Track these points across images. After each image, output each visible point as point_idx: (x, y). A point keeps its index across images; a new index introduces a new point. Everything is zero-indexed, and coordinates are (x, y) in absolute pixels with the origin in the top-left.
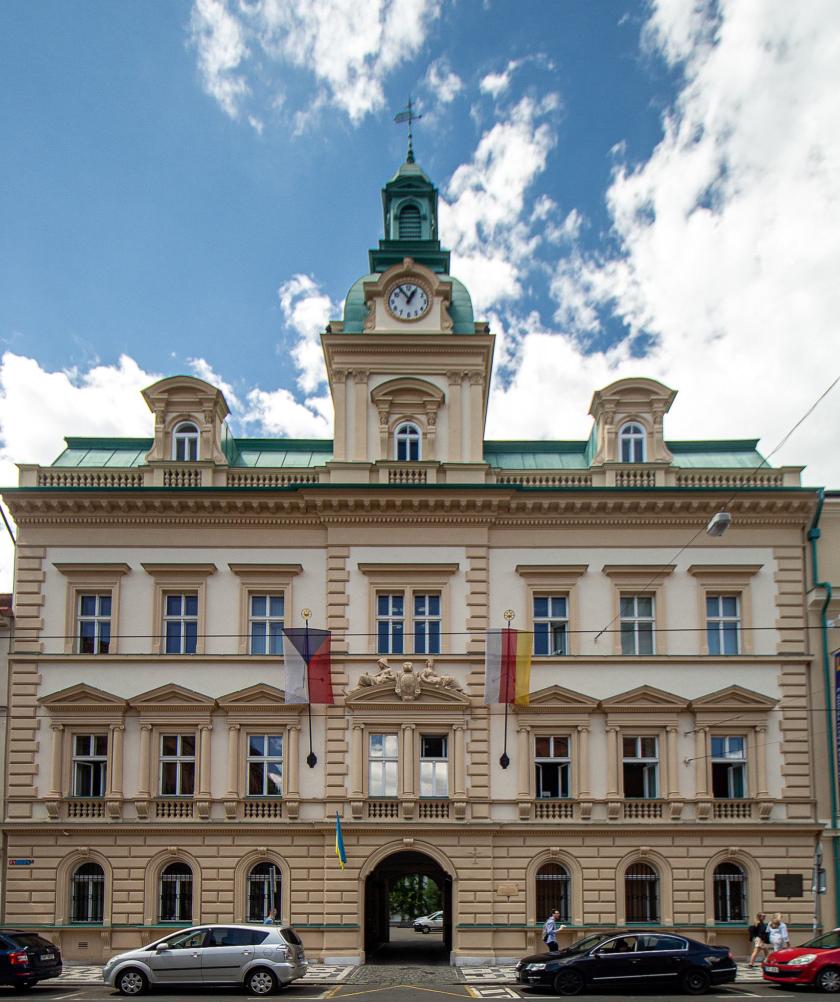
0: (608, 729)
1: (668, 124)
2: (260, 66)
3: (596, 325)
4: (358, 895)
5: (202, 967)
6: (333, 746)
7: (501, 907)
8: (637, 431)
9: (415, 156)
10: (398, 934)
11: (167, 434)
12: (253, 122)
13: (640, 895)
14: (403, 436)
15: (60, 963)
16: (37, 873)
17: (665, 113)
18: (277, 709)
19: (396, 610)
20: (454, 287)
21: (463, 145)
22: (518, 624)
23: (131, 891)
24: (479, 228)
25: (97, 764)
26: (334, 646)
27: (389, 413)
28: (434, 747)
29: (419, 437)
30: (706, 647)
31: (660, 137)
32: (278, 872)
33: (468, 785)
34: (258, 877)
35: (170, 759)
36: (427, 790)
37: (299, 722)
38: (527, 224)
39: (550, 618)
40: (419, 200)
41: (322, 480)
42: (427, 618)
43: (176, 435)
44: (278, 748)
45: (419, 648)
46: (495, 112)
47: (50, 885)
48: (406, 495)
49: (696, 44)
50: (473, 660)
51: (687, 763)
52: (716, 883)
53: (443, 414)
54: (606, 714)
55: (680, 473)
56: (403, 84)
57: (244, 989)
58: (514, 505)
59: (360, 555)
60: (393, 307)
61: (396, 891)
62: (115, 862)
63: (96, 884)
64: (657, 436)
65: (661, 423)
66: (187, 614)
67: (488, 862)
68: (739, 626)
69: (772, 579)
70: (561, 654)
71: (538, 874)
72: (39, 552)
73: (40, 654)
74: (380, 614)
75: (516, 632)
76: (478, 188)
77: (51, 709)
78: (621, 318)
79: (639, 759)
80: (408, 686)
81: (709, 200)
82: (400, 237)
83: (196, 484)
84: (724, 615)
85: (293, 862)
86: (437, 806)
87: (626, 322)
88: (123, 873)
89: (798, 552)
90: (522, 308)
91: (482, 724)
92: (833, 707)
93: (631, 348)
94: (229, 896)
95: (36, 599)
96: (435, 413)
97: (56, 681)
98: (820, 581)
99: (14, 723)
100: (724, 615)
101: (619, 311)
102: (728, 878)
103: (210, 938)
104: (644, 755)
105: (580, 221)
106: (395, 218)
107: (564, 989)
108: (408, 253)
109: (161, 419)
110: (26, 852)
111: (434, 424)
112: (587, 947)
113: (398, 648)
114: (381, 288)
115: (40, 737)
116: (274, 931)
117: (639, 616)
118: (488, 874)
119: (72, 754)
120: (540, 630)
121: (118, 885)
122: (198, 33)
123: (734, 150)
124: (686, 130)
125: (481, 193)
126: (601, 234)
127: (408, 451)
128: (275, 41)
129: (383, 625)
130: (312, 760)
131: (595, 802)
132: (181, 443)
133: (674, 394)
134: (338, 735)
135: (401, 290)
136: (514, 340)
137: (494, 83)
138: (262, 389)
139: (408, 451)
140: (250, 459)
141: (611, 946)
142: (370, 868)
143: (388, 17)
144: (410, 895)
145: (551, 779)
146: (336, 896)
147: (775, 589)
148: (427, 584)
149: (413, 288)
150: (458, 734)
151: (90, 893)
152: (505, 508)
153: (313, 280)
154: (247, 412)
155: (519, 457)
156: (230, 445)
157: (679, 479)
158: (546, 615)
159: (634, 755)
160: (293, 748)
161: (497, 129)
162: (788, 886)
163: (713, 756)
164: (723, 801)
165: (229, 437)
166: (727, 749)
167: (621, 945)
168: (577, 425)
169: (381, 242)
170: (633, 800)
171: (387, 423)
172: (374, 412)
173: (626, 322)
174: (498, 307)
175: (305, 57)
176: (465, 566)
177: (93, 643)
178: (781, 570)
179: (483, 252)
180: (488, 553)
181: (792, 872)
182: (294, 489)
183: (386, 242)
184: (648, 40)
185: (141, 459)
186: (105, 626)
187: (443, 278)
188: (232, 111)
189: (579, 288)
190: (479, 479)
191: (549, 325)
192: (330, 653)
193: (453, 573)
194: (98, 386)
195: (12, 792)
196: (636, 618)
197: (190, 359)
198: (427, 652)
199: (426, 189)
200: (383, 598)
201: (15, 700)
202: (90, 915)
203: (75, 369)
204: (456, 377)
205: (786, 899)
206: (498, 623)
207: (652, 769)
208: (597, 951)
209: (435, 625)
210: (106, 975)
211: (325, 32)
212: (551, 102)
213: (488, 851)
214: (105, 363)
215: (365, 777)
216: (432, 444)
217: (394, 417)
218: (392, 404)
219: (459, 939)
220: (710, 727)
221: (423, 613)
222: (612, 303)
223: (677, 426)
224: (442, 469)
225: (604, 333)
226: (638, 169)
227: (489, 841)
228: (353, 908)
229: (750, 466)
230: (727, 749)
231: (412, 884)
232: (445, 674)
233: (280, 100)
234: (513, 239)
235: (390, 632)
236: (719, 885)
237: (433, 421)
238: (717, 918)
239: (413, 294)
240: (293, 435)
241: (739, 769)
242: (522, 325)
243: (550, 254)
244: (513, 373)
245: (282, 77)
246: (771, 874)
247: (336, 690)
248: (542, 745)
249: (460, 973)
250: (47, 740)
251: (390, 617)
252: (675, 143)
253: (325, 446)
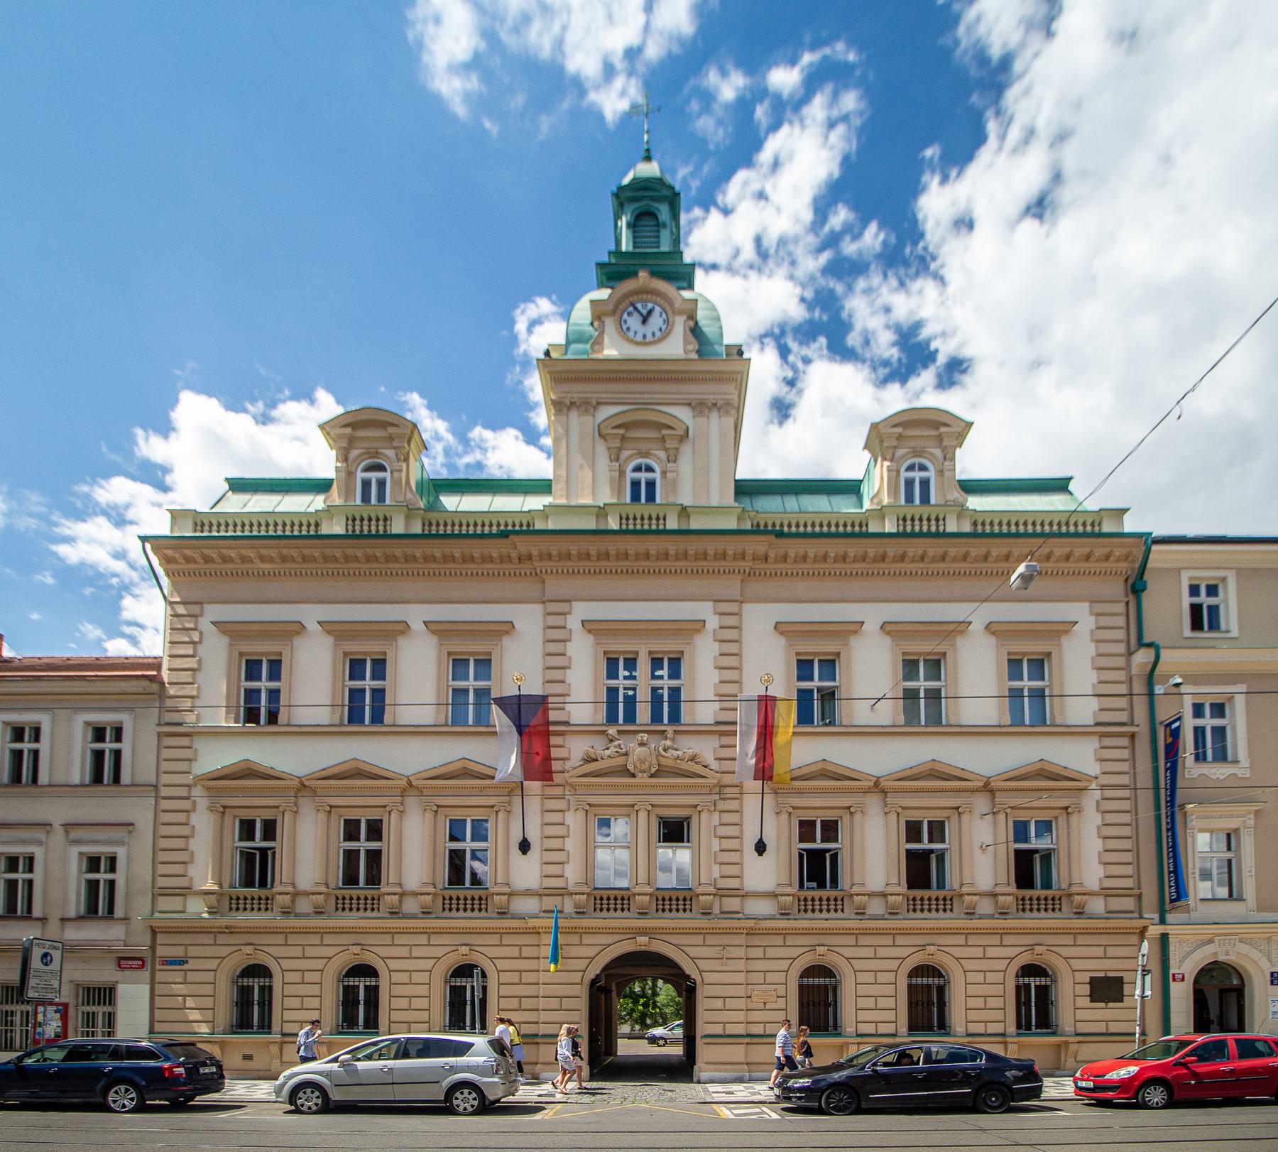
0: (887, 810)
1: (992, 127)
2: (498, 60)
3: (894, 353)
4: (582, 1003)
5: (391, 1080)
6: (551, 831)
7: (754, 1016)
8: (923, 468)
9: (652, 153)
10: (627, 1048)
11: (350, 474)
12: (487, 124)
13: (925, 1000)
14: (637, 475)
15: (222, 1077)
16: (192, 977)
17: (990, 113)
18: (482, 791)
19: (627, 673)
20: (700, 305)
21: (743, 147)
22: (777, 690)
23: (305, 994)
24: (758, 240)
25: (264, 851)
26: (553, 716)
27: (620, 449)
28: (674, 831)
29: (657, 475)
30: (1009, 717)
31: (981, 139)
32: (484, 975)
33: (716, 874)
34: (459, 982)
35: (352, 845)
36: (667, 880)
37: (509, 803)
38: (817, 234)
39: (815, 684)
40: (656, 205)
41: (539, 526)
42: (666, 683)
43: (360, 475)
44: (483, 832)
45: (656, 717)
46: (786, 110)
47: (208, 989)
48: (641, 541)
49: (1027, 31)
50: (723, 729)
51: (983, 848)
52: (1018, 988)
53: (686, 450)
55: (977, 518)
56: (670, 81)
57: (445, 1108)
59: (582, 611)
60: (625, 327)
61: (625, 997)
62: (286, 964)
63: (262, 989)
64: (947, 474)
65: (953, 459)
66: (373, 678)
67: (741, 965)
68: (1047, 693)
69: (1088, 637)
70: (832, 723)
71: (801, 977)
72: (195, 609)
74: (608, 678)
75: (774, 699)
76: (761, 196)
77: (208, 789)
78: (928, 342)
79: (925, 845)
80: (642, 761)
81: (1039, 207)
82: (635, 247)
83: (385, 531)
84: (1029, 679)
85: (502, 964)
87: (933, 346)
88: (296, 977)
90: (807, 332)
91: (732, 805)
92: (1162, 784)
93: (939, 376)
94: (423, 1003)
95: (191, 663)
96: (677, 449)
97: (215, 758)
98: (1147, 640)
99: (165, 804)
100: (1029, 679)
101: (925, 333)
102: (1034, 982)
103: (404, 1051)
104: (931, 841)
105: (882, 237)
106: (629, 225)
107: (834, 1108)
108: (644, 266)
109: (344, 456)
110: (178, 952)
111: (675, 462)
112: (862, 1060)
113: (631, 717)
114: (611, 307)
115: (195, 819)
116: (479, 1041)
117: (926, 680)
118: (740, 978)
119: (234, 841)
120: (804, 698)
121: (289, 990)
122: (425, 22)
123: (1071, 156)
124: (1014, 134)
125: (763, 203)
126: (908, 250)
127: (643, 491)
128: (516, 30)
129: (612, 691)
130: (525, 846)
131: (871, 895)
132: (366, 484)
133: (969, 425)
134: (556, 817)
135: (636, 309)
136: (794, 368)
137: (784, 78)
138: (485, 427)
139: (643, 491)
140: (450, 502)
141: (890, 1059)
142: (595, 969)
143: (655, 8)
144: (642, 1001)
145: (818, 868)
146: (554, 1003)
147: (1091, 649)
148: (666, 646)
149: (650, 306)
150: (703, 815)
151: (256, 997)
153: (554, 303)
154: (466, 453)
155: (778, 498)
156: (426, 486)
157: (975, 524)
158: (812, 679)
159: (919, 840)
160: (504, 831)
161: (785, 129)
162: (1107, 989)
163: (1016, 841)
164: (1027, 893)
165: (425, 476)
166: (1033, 833)
167: (904, 1056)
168: (851, 462)
169: (610, 253)
170: (918, 893)
171: (617, 460)
172: (601, 448)
173: (933, 346)
174: (777, 331)
175: (553, 49)
176: (713, 623)
177: (260, 711)
178: (1098, 628)
179: (760, 270)
180: (741, 609)
182: (504, 535)
183: (617, 253)
184: (969, 30)
185: (316, 503)
186: (274, 695)
187: (686, 294)
188: (461, 111)
189: (874, 309)
190: (732, 524)
191: (841, 352)
192: (548, 723)
193: (698, 631)
194: (287, 423)
195: (162, 882)
196: (922, 684)
197: (401, 393)
198: (666, 720)
199: (666, 192)
200: (612, 664)
201: (165, 779)
203: (260, 405)
204: (700, 407)
205: (1103, 1005)
206: (753, 689)
207: (941, 858)
208: (875, 1064)
209: (675, 692)
210: (278, 1091)
211: (578, 21)
212: (850, 101)
213: (741, 952)
214: (296, 397)
215: (589, 863)
216: (673, 486)
217: (625, 454)
218: (623, 438)
219: (704, 1052)
220: (1012, 808)
221: (661, 677)
222: (918, 326)
223: (973, 460)
224: (684, 512)
225: (904, 361)
226: (953, 173)
227: (741, 940)
229: (1061, 508)
230: (1033, 833)
231: (643, 990)
232: (690, 746)
233: (519, 100)
234: (799, 251)
235: (621, 698)
236: (1022, 991)
237: (673, 458)
238: (1019, 1026)
239: (650, 312)
240: (520, 474)
241: (1047, 856)
242: (805, 351)
243: (846, 270)
244: (791, 406)
245: (526, 77)
247: (556, 765)
248: (806, 829)
249: (706, 1090)
250: (203, 823)
251: (621, 683)
252: (1000, 149)
253: (542, 487)
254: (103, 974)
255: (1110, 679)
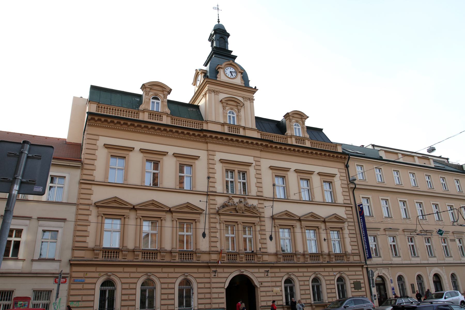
0: (173, 219)
53: (242, 110)
54: (220, 215)
58: (269, 146)
59: (103, 140)
73: (94, 181)
86: (114, 252)
89: (344, 171)
152: (267, 146)
172: (221, 105)
181: (358, 280)
202: (147, 306)
228: (263, 299)
246: (352, 282)
254: (49, 284)
255: (88, 165)
